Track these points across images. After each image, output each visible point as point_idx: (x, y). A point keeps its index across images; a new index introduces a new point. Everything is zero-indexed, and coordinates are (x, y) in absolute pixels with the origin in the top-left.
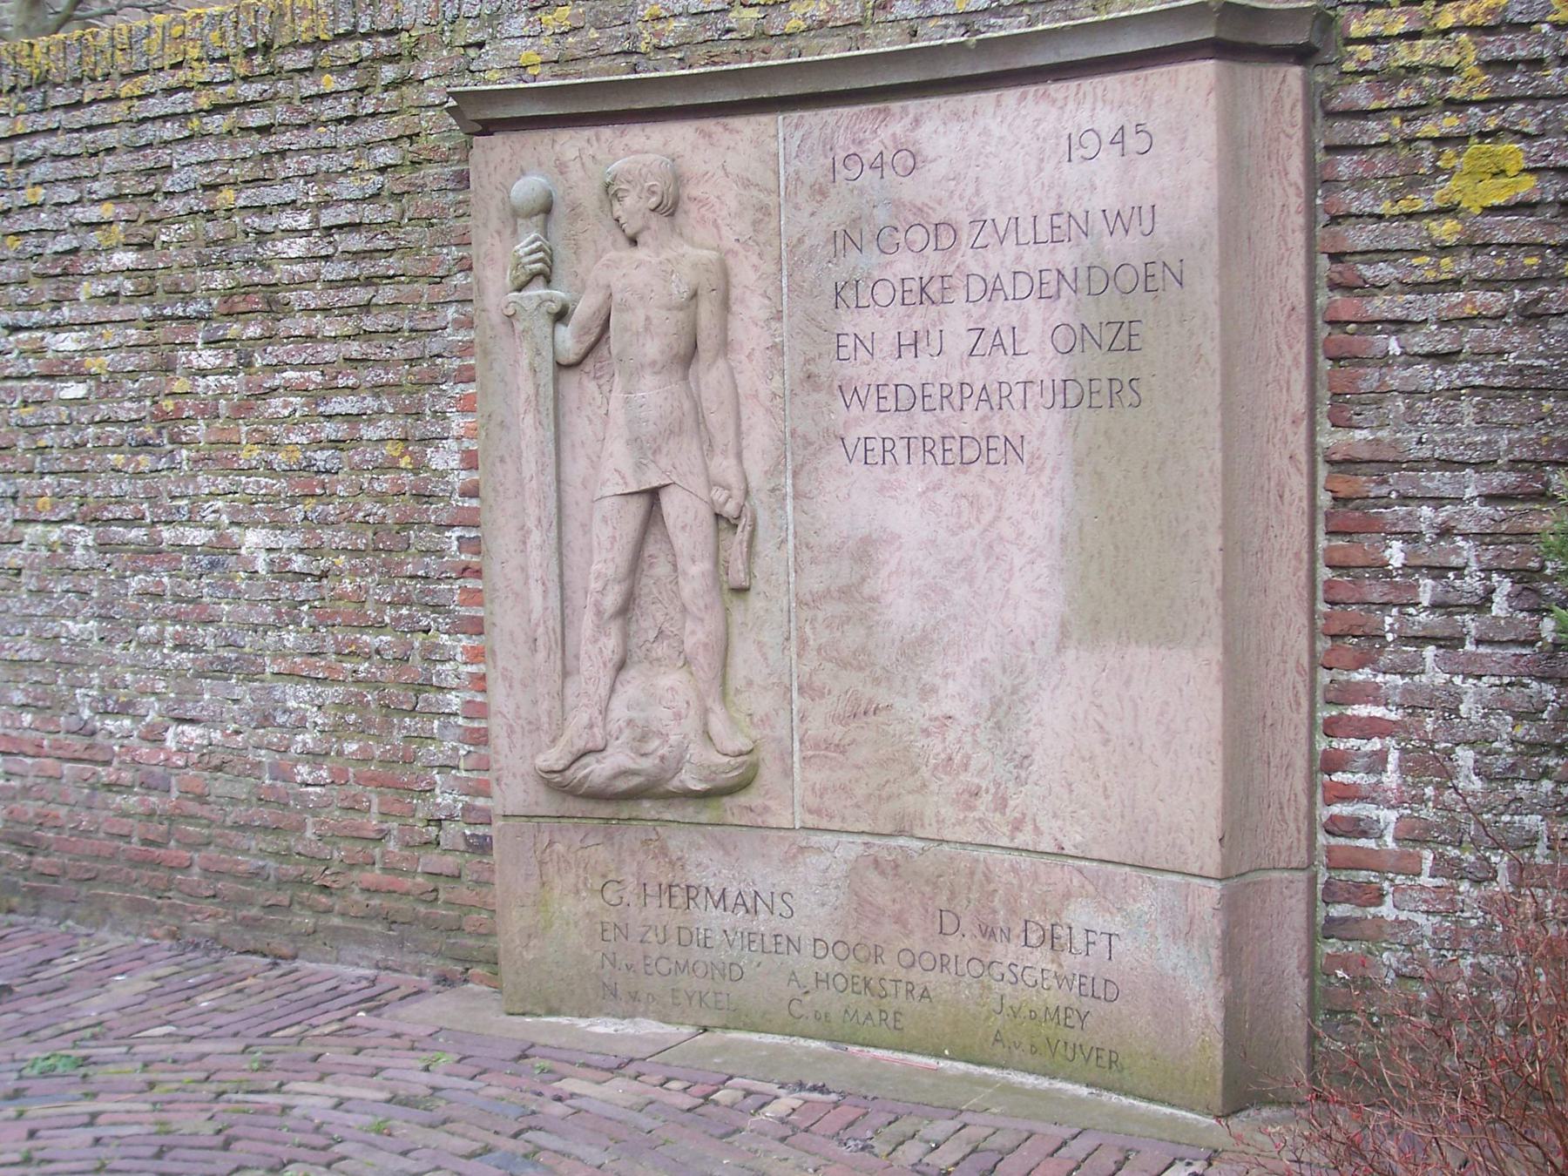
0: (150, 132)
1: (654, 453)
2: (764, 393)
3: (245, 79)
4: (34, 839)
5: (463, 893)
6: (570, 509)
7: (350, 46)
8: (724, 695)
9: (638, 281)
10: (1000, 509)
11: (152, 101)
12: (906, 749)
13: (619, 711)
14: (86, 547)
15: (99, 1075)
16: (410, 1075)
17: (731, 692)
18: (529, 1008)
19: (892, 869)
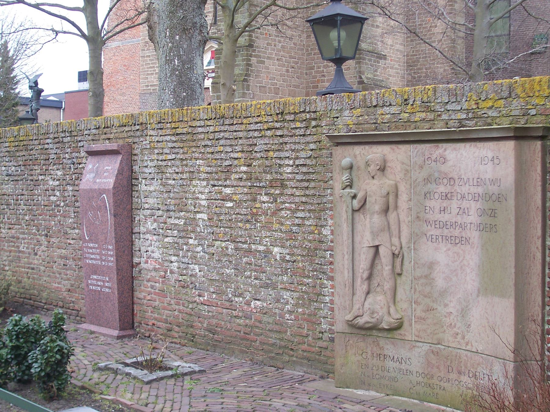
0: (251, 134)
1: (377, 236)
2: (406, 221)
3: (276, 121)
4: (215, 330)
5: (328, 353)
6: (356, 249)
7: (304, 115)
8: (394, 303)
9: (373, 188)
10: (464, 257)
11: (252, 125)
12: (440, 321)
13: (367, 305)
14: (232, 249)
15: (225, 393)
16: (304, 400)
17: (396, 302)
18: (341, 386)
19: (436, 353)
